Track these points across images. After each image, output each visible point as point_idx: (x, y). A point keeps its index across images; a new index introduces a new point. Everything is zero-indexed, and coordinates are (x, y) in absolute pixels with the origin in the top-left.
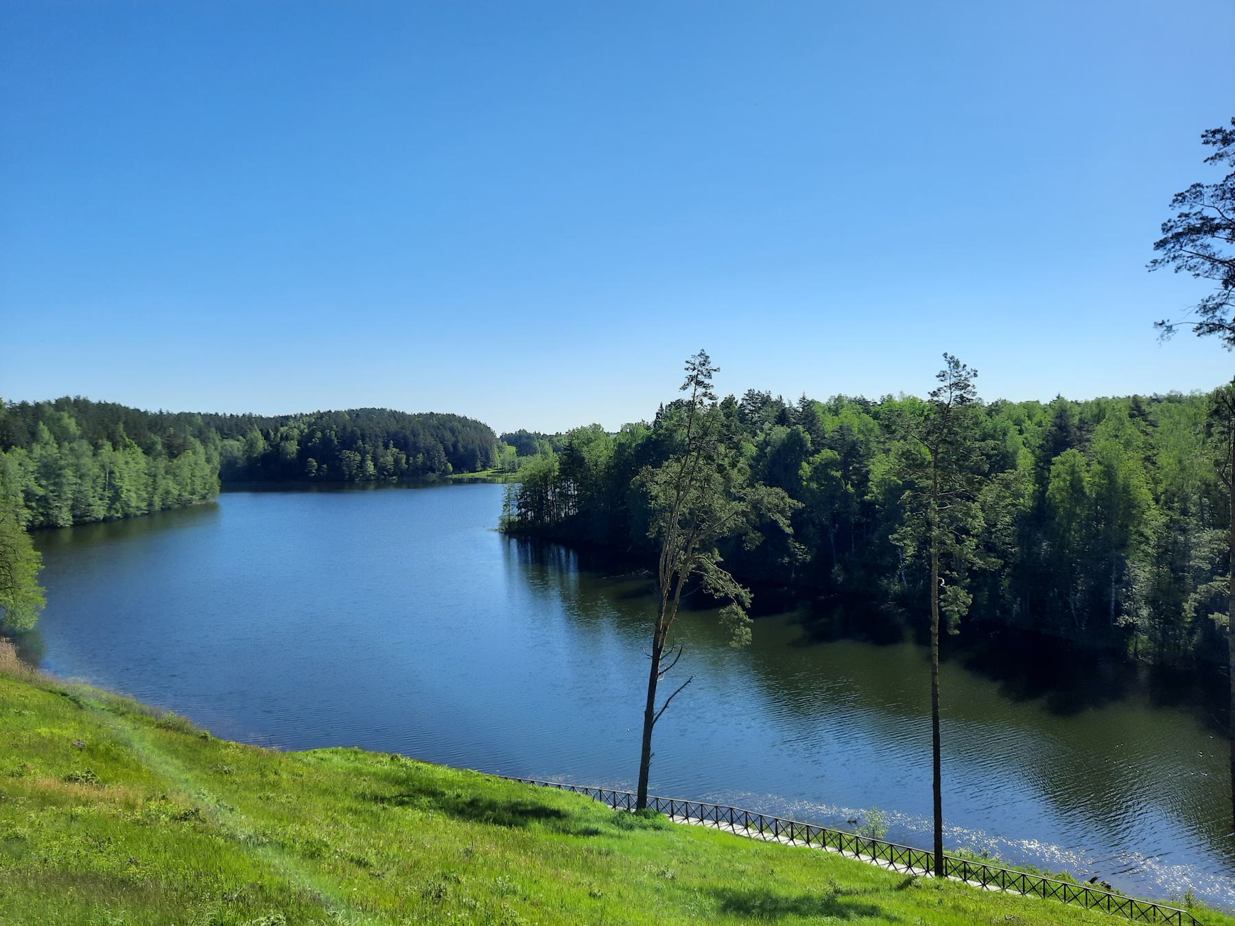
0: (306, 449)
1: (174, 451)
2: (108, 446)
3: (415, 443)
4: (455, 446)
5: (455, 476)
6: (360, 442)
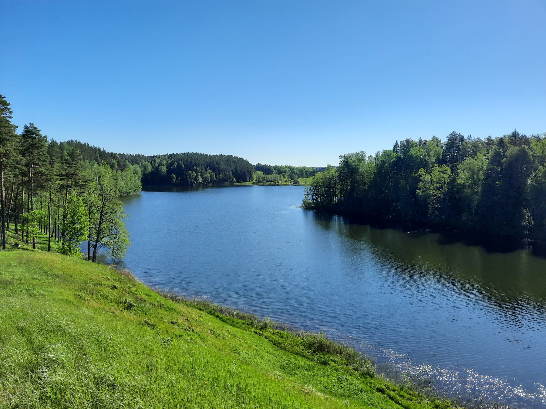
0: (170, 171)
1: (122, 168)
2: (96, 164)
3: (219, 168)
4: (236, 169)
5: (237, 184)
6: (195, 167)
